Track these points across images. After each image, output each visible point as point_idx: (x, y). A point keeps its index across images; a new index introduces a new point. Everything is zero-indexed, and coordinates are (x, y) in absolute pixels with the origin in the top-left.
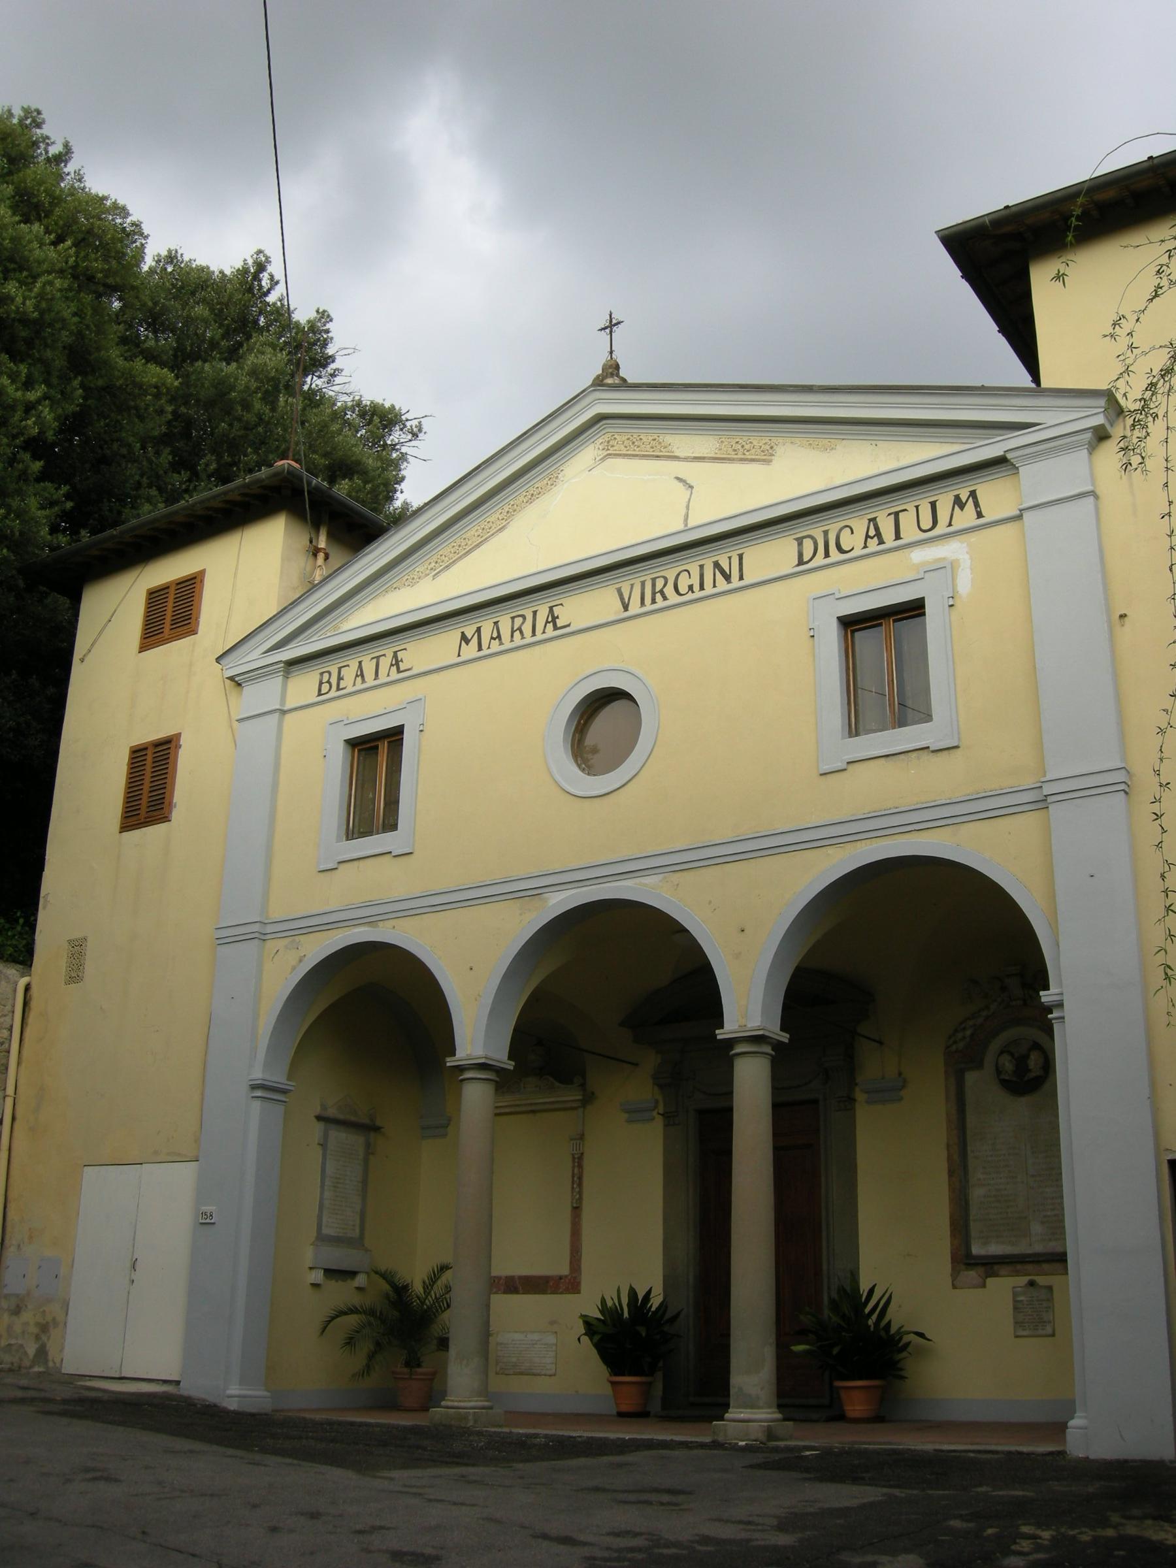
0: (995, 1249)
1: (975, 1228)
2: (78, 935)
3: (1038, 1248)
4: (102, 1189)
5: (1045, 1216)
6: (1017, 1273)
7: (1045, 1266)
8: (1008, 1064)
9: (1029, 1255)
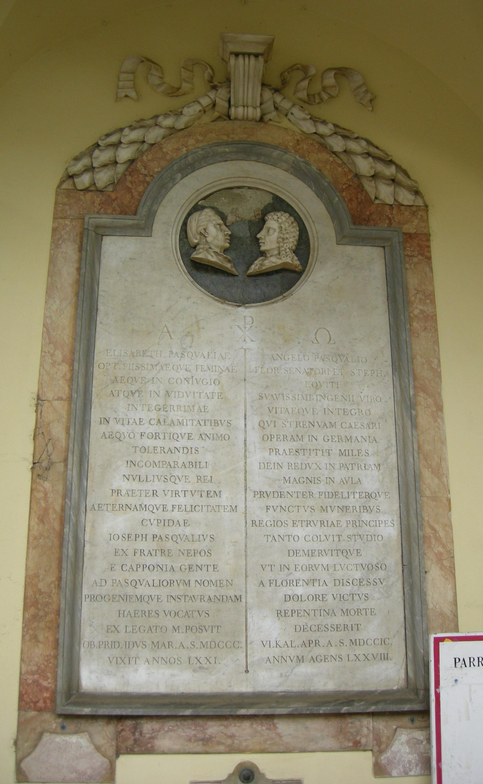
0: (146, 677)
1: (92, 619)
2: (456, 678)
3: (267, 680)
4: (384, 724)
5: (288, 598)
6: (207, 746)
7: (285, 728)
8: (212, 236)
9: (243, 700)
